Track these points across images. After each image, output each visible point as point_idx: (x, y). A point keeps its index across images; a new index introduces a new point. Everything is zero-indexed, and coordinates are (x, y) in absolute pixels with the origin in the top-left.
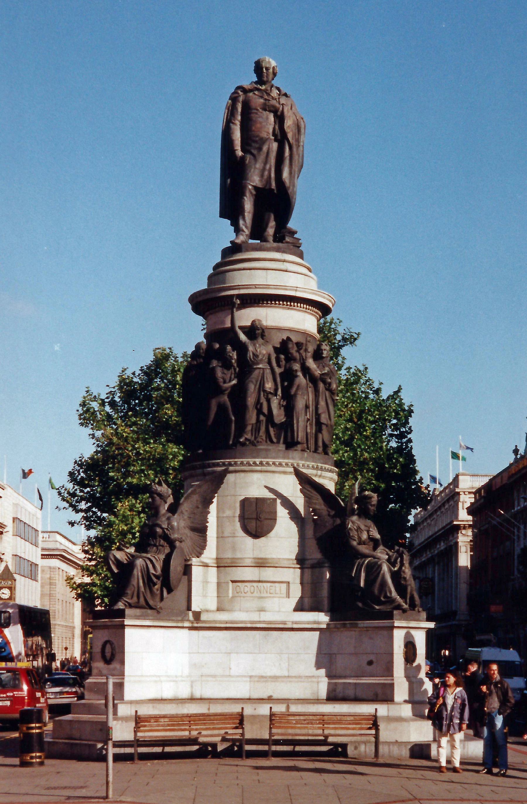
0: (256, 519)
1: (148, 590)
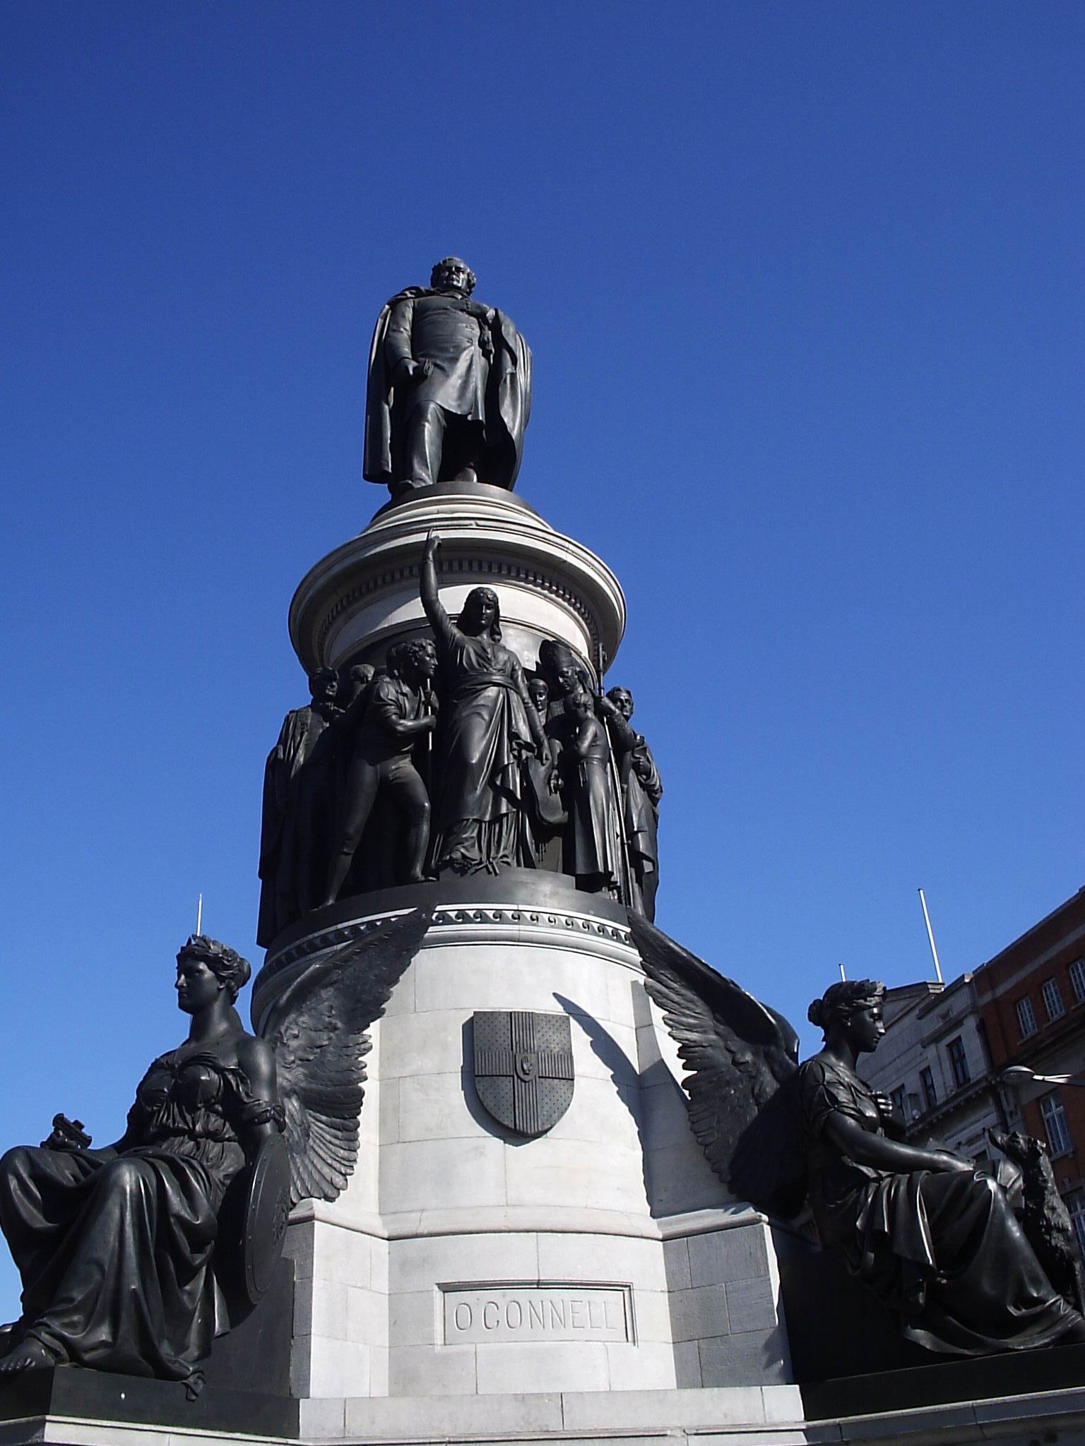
0: (508, 1080)
1: (156, 1290)
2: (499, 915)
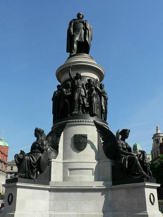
0: (79, 143)
2: (86, 121)
